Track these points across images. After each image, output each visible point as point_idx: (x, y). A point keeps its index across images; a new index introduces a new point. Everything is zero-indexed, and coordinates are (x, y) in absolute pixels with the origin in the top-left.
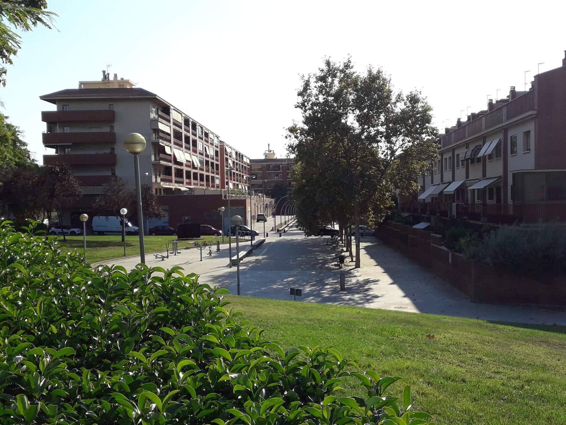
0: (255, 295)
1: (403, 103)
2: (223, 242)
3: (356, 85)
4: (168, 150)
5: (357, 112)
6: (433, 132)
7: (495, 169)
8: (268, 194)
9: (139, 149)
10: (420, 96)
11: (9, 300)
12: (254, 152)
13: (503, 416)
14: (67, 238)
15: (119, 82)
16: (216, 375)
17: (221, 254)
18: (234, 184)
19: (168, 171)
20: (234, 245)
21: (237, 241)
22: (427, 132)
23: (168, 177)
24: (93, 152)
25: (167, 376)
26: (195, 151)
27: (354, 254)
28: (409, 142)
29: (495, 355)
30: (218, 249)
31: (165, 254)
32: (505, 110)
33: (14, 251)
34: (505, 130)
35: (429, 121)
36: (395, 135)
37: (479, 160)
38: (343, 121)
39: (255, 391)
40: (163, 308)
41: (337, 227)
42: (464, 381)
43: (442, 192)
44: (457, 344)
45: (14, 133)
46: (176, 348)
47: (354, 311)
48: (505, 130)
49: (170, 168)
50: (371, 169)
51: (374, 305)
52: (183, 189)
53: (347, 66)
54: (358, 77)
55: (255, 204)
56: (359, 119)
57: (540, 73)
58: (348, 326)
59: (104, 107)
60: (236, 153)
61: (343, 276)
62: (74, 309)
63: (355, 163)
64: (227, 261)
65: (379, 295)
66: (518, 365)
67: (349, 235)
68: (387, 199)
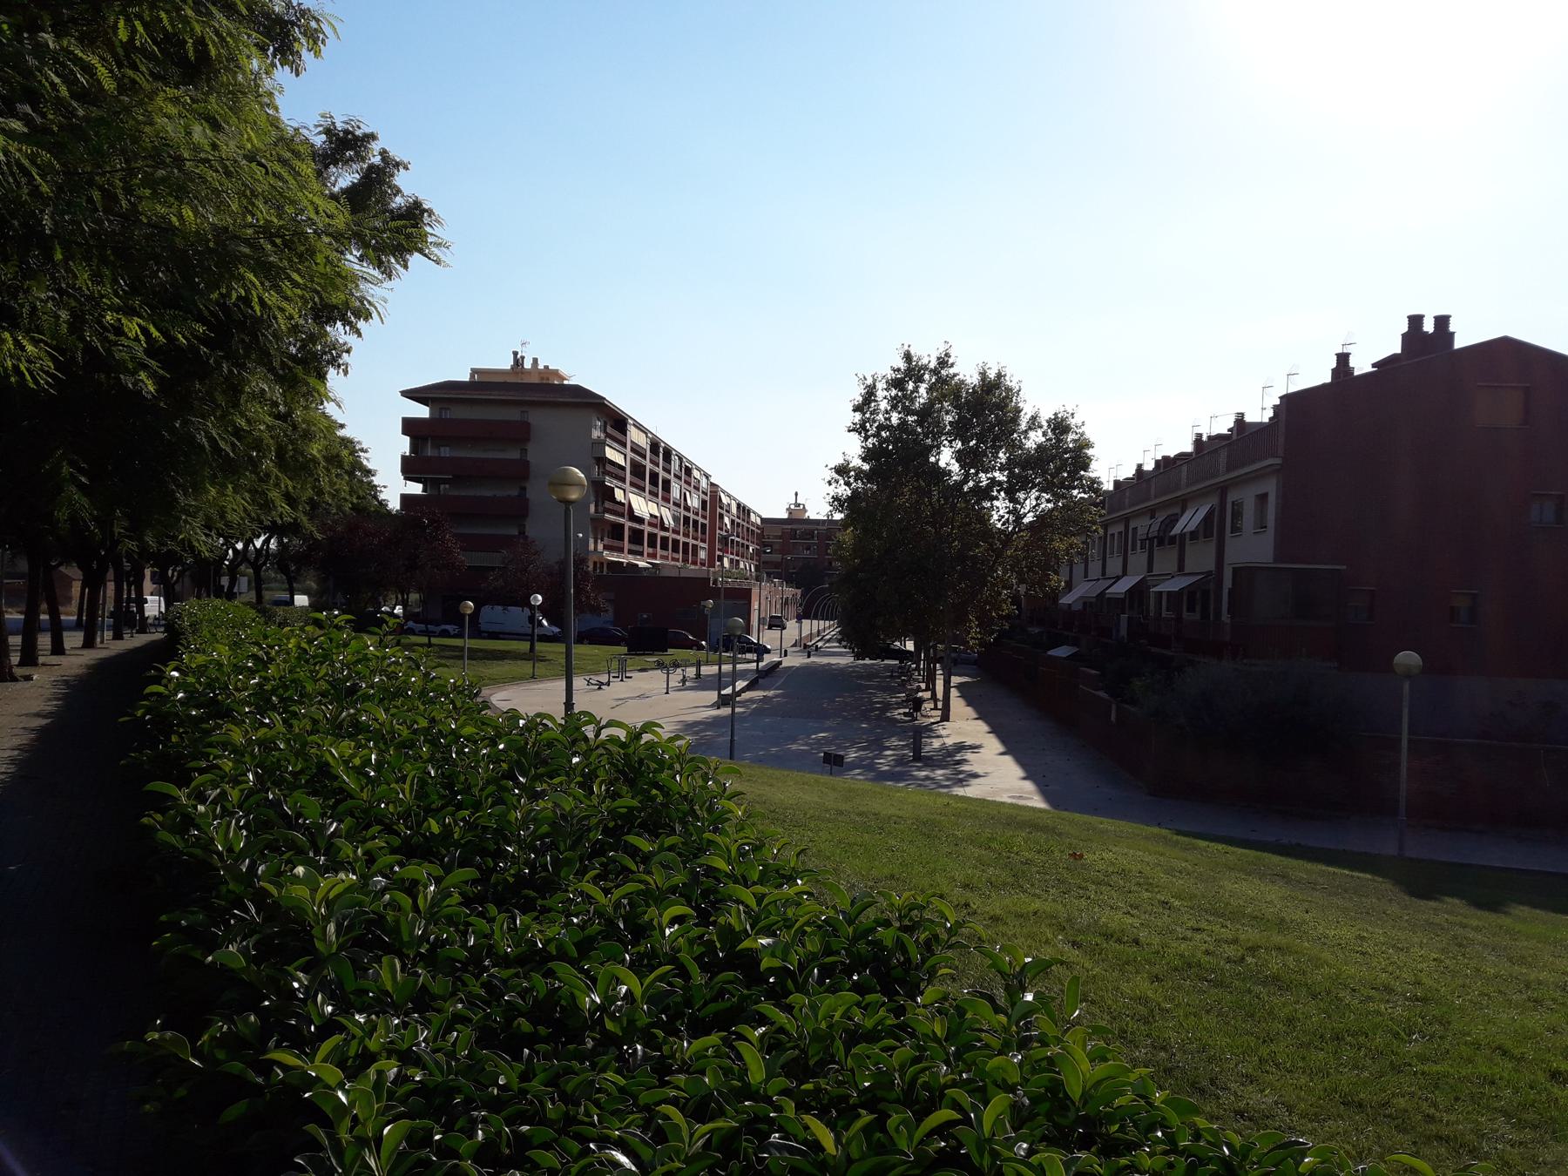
0: (760, 761)
1: (1040, 432)
2: (707, 663)
3: (957, 396)
4: (619, 495)
5: (959, 445)
6: (1094, 486)
7: (1201, 559)
8: (790, 580)
9: (574, 495)
10: (1072, 422)
11: (354, 767)
12: (770, 506)
13: (1208, 1012)
14: (434, 640)
15: (540, 372)
16: (731, 936)
17: (701, 683)
18: (731, 561)
19: (616, 531)
20: (726, 668)
21: (734, 662)
22: (1082, 486)
23: (616, 543)
24: (489, 493)
25: (640, 931)
26: (666, 499)
27: (940, 695)
28: (1048, 501)
29: (1192, 897)
30: (698, 675)
31: (604, 678)
32: (1223, 455)
33: (358, 673)
34: (1223, 490)
35: (1086, 467)
36: (1023, 488)
37: (1173, 540)
38: (932, 459)
39: (801, 971)
40: (628, 801)
41: (910, 646)
42: (1137, 942)
43: (1102, 594)
44: (1123, 873)
45: (353, 452)
46: (657, 879)
47: (939, 800)
48: (1223, 490)
49: (622, 526)
50: (978, 546)
51: (973, 790)
52: (642, 564)
53: (943, 362)
54: (962, 382)
55: (766, 597)
56: (960, 456)
57: (1291, 390)
58: (927, 829)
59: (512, 414)
60: (739, 505)
61: (920, 734)
62: (467, 790)
63: (950, 534)
64: (712, 696)
65: (980, 772)
66: (1236, 916)
67: (931, 660)
68: (1004, 601)
